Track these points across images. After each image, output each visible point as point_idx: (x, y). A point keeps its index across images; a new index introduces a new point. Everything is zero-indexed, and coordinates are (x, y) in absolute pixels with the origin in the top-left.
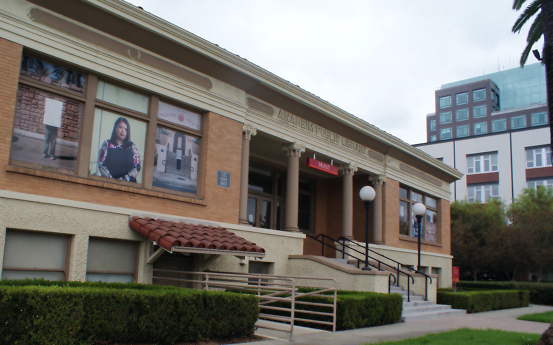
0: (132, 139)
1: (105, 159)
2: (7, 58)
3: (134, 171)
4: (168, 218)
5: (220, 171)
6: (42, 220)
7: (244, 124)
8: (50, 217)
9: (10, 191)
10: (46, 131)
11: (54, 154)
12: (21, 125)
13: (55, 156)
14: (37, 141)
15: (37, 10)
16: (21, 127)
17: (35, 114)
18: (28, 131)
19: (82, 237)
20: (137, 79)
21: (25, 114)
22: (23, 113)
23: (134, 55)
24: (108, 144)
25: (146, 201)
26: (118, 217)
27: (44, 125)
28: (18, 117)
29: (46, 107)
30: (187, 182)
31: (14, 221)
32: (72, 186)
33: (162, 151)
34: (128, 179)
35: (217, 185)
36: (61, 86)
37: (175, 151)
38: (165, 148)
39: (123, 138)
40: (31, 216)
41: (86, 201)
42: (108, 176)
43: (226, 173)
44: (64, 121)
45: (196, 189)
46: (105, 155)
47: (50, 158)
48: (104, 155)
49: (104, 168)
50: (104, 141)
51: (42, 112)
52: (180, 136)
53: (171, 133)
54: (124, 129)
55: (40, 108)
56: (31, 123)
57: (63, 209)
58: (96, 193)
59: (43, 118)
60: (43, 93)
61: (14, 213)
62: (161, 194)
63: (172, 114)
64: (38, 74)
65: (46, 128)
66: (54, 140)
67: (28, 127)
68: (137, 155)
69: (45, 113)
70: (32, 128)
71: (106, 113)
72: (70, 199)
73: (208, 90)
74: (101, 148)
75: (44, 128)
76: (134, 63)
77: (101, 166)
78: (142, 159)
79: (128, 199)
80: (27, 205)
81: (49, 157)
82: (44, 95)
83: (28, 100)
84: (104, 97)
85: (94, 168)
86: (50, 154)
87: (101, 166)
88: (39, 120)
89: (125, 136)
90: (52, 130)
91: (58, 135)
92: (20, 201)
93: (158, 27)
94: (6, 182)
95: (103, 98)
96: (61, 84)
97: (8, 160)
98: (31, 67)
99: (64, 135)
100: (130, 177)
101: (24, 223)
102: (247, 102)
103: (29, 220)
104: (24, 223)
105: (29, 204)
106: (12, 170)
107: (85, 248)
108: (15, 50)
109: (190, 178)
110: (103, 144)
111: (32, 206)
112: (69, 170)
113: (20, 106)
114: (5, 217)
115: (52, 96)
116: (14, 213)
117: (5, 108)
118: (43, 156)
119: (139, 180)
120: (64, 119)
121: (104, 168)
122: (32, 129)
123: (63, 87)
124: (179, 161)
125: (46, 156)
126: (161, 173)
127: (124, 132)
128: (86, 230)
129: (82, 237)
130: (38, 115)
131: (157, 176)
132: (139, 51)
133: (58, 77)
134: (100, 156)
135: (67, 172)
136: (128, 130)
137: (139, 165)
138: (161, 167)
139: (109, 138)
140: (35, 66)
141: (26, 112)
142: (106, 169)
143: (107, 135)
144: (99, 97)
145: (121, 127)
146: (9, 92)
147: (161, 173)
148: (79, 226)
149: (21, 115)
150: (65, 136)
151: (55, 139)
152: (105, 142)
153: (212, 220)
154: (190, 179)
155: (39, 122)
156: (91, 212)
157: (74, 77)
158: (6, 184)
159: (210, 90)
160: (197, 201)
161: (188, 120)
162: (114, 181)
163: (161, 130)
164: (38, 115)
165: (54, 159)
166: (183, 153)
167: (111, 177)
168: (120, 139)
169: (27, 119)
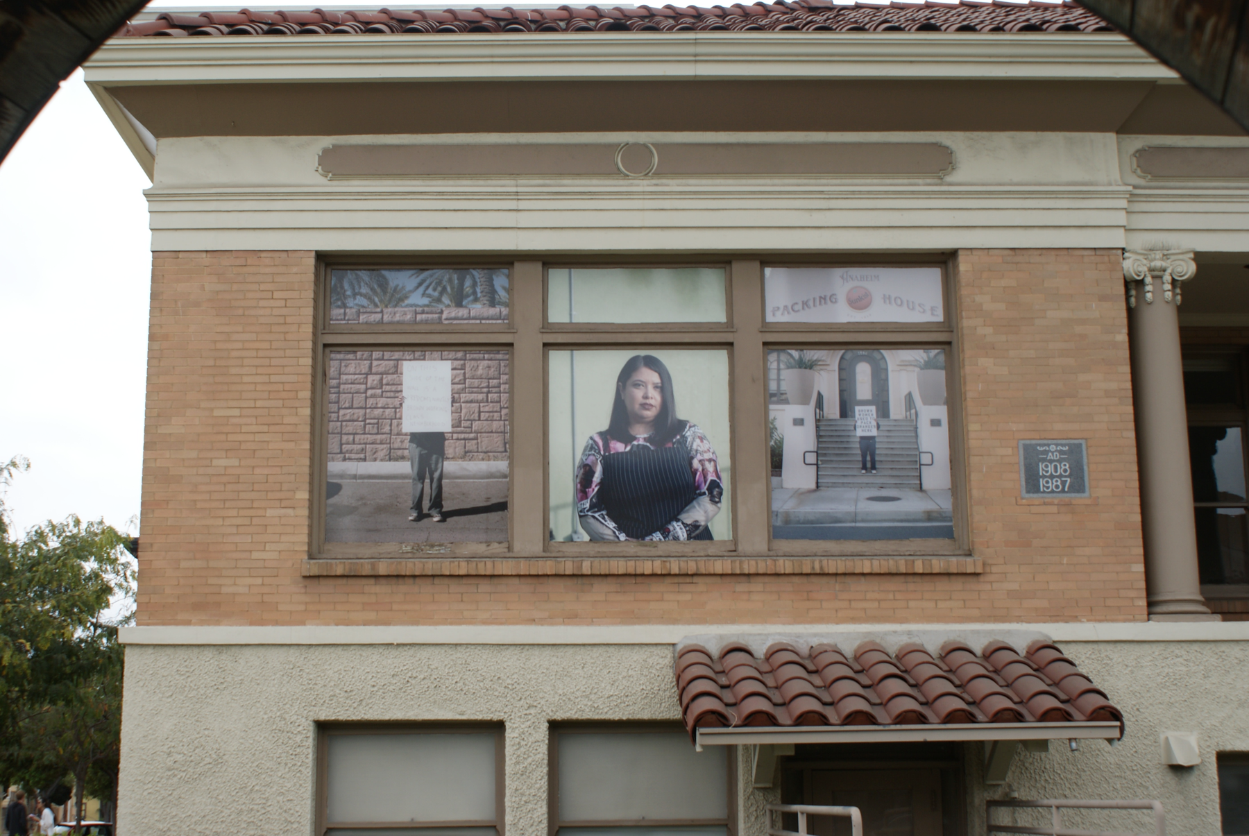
0: (681, 412)
1: (596, 489)
2: (276, 295)
3: (699, 504)
4: (815, 635)
5: (1034, 442)
6: (403, 690)
7: (1127, 249)
8: (424, 679)
9: (317, 625)
10: (412, 450)
11: (442, 507)
12: (344, 450)
13: (444, 510)
14: (389, 481)
15: (336, 148)
16: (345, 456)
17: (377, 412)
18: (365, 460)
19: (523, 726)
20: (548, 231)
21: (351, 418)
22: (348, 417)
23: (638, 162)
24: (601, 444)
25: (734, 592)
26: (637, 656)
27: (406, 434)
28: (336, 431)
29: (405, 387)
30: (911, 505)
31: (330, 702)
32: (485, 586)
33: (799, 422)
34: (682, 533)
35: (1027, 496)
36: (440, 318)
37: (845, 411)
38: (807, 412)
39: (650, 414)
40: (373, 684)
41: (532, 621)
42: (612, 538)
43: (1063, 445)
44: (459, 410)
45: (951, 521)
46: (597, 477)
47: (430, 519)
48: (593, 476)
49: (596, 515)
50: (588, 438)
51: (397, 402)
52: (860, 361)
53: (823, 358)
54: (650, 388)
55: (388, 394)
56: (370, 438)
57: (460, 654)
58: (564, 596)
59: (400, 418)
60: (392, 353)
61: (328, 680)
62: (787, 562)
63: (821, 297)
64: (376, 306)
65: (410, 442)
66: (436, 470)
67: (363, 449)
68: (707, 456)
69: (403, 404)
70: (374, 451)
71: (582, 356)
72: (485, 622)
73: (939, 181)
74: (582, 459)
75: (407, 444)
76: (644, 185)
77: (588, 511)
78: (724, 462)
79: (671, 596)
80: (361, 655)
81: (429, 516)
82: (397, 355)
83: (356, 382)
84: (574, 313)
85: (564, 523)
86: (430, 509)
87: (588, 511)
88: (391, 425)
89: (658, 408)
90: (430, 445)
91: (446, 452)
92: (340, 648)
93: (1007, 60)
94: (306, 603)
95: (571, 315)
96: (442, 312)
97: (306, 548)
98: (355, 295)
99: (465, 447)
100: (685, 525)
101: (355, 705)
102: (1135, 166)
103: (369, 695)
104: (355, 705)
105: (366, 652)
106: (315, 572)
107: (538, 756)
108: (295, 270)
109: (921, 489)
110: (587, 447)
111: (374, 656)
112: (488, 544)
113: (338, 402)
114: (306, 693)
115: (419, 353)
116: (328, 680)
117: (286, 420)
118: (411, 518)
119: (721, 529)
120: (461, 406)
121: (596, 515)
122: (375, 453)
123: (446, 319)
124: (868, 445)
125: (417, 517)
126: (802, 494)
127: (650, 395)
128: (535, 704)
129: (523, 726)
130: (387, 413)
131: (784, 504)
132: (652, 144)
133: (429, 296)
134: (581, 483)
135: (482, 549)
136: (665, 387)
137: (715, 486)
138: (798, 475)
139: (604, 425)
140: (364, 290)
141: (353, 414)
142: (604, 518)
143: (597, 417)
144: (558, 314)
145: (639, 385)
146: (293, 378)
147: (801, 495)
148: (514, 695)
149: (341, 425)
150: (466, 452)
151: (440, 465)
152: (591, 442)
153: (1019, 619)
154: (920, 494)
155: (391, 430)
156: (547, 652)
157: (474, 285)
158: (306, 610)
159: (948, 179)
160: (954, 564)
161: (887, 299)
162: (633, 547)
163: (783, 357)
164: (387, 413)
165: (443, 520)
166: (883, 412)
167: (622, 537)
168: (640, 419)
169: (358, 431)
